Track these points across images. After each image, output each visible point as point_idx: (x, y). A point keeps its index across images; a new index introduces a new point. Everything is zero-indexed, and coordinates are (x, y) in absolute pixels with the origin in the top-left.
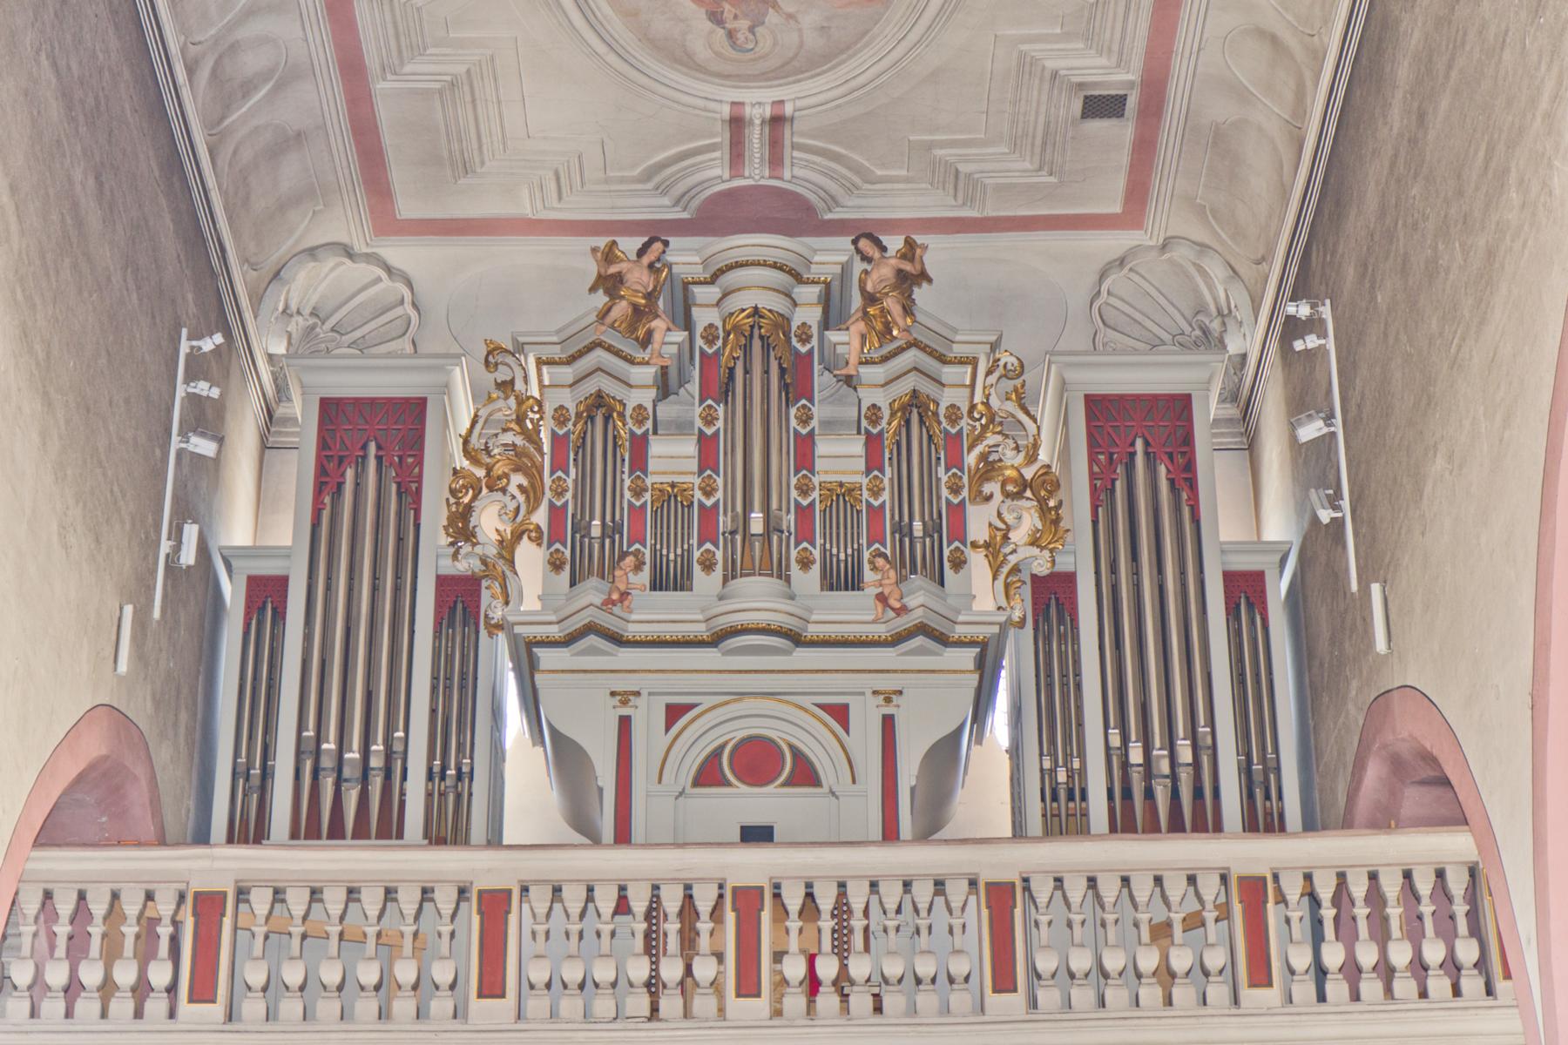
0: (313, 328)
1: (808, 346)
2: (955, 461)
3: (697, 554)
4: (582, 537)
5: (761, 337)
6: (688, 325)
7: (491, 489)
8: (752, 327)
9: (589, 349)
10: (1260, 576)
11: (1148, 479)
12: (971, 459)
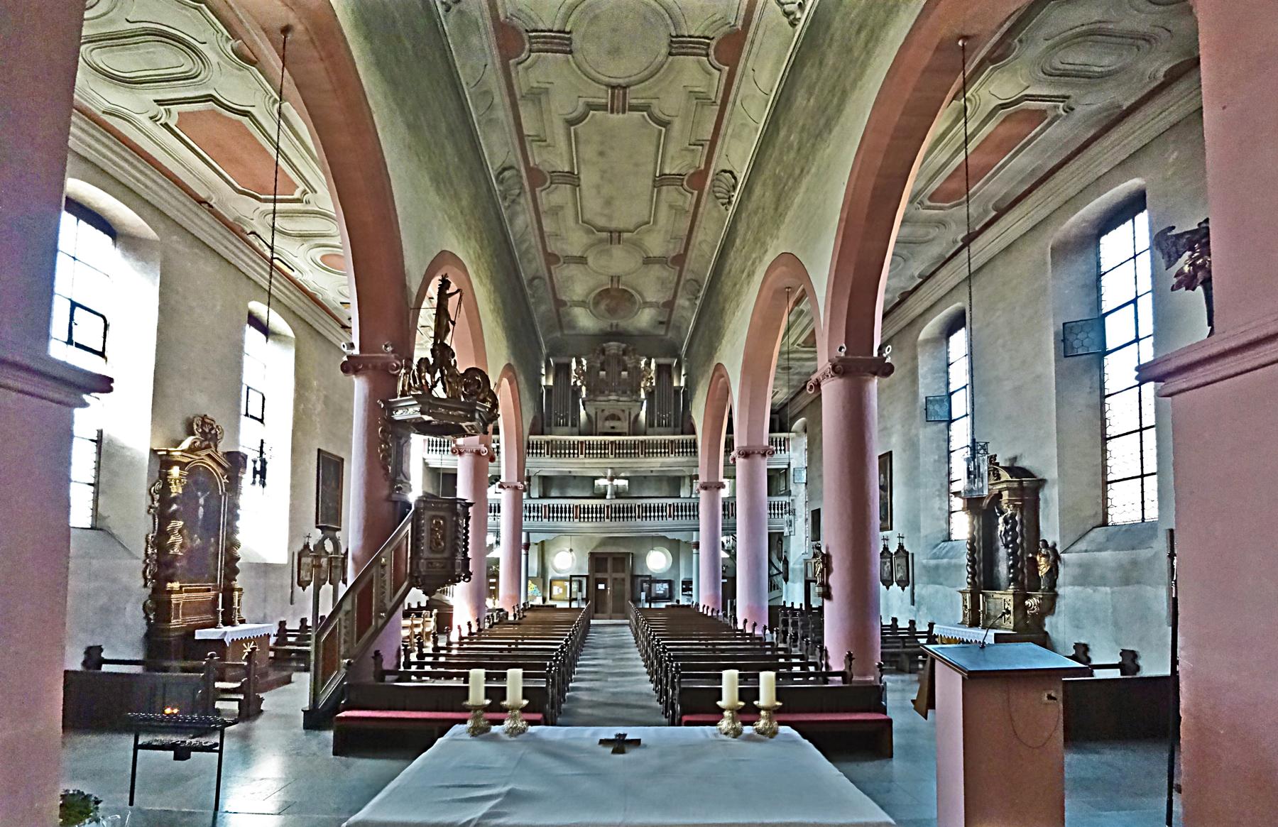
11: (665, 376)
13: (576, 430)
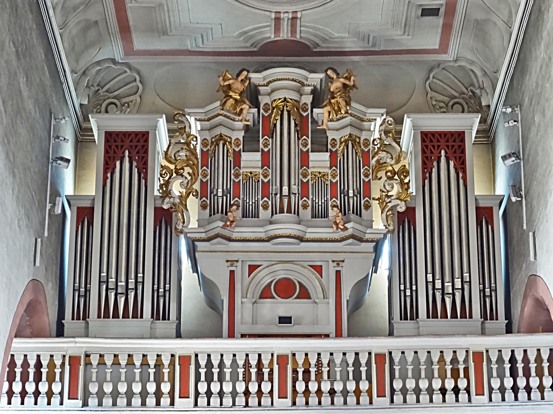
0: (99, 90)
1: (307, 113)
2: (367, 163)
3: (261, 202)
4: (214, 196)
5: (287, 110)
6: (257, 106)
7: (177, 173)
8: (283, 106)
9: (216, 116)
10: (491, 209)
11: (445, 166)
12: (373, 162)
13: (169, 326)
